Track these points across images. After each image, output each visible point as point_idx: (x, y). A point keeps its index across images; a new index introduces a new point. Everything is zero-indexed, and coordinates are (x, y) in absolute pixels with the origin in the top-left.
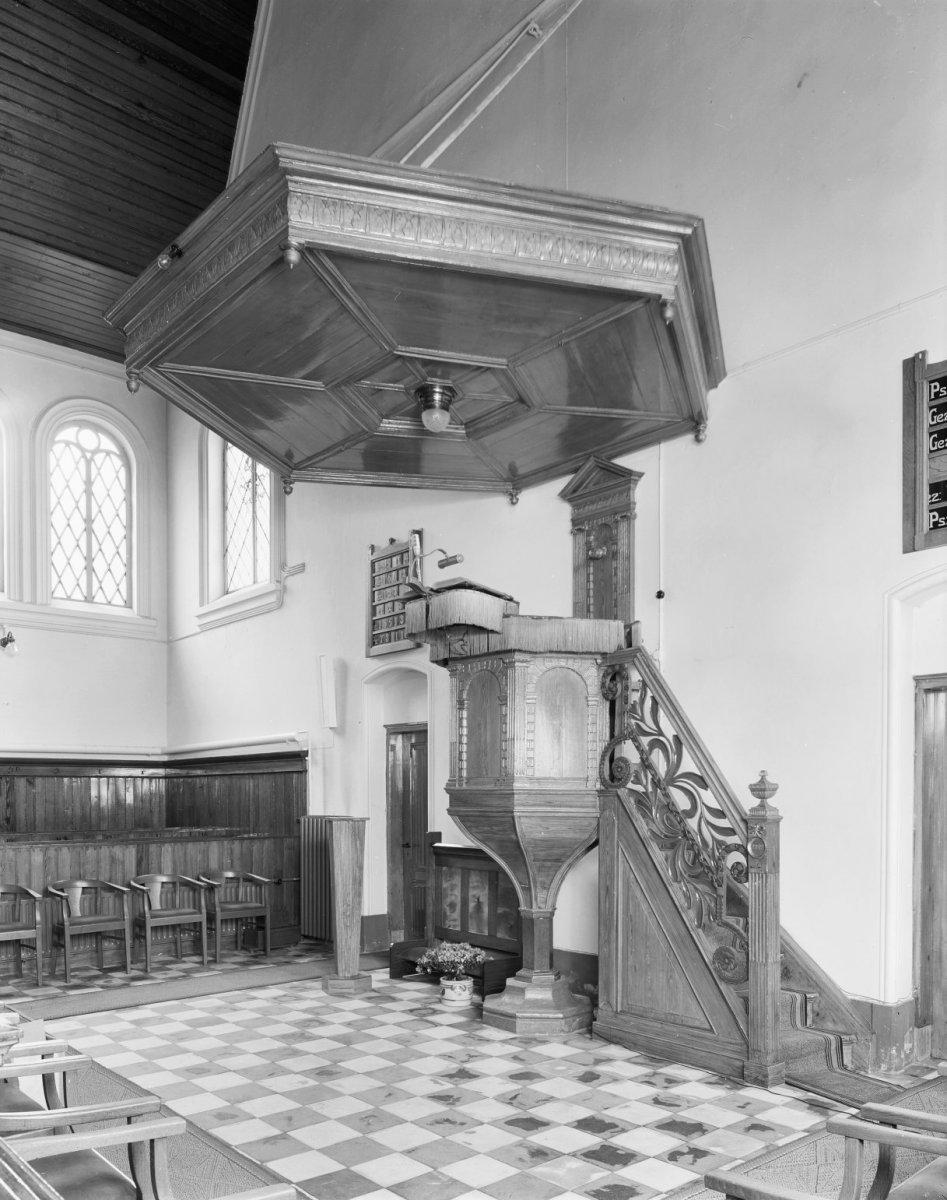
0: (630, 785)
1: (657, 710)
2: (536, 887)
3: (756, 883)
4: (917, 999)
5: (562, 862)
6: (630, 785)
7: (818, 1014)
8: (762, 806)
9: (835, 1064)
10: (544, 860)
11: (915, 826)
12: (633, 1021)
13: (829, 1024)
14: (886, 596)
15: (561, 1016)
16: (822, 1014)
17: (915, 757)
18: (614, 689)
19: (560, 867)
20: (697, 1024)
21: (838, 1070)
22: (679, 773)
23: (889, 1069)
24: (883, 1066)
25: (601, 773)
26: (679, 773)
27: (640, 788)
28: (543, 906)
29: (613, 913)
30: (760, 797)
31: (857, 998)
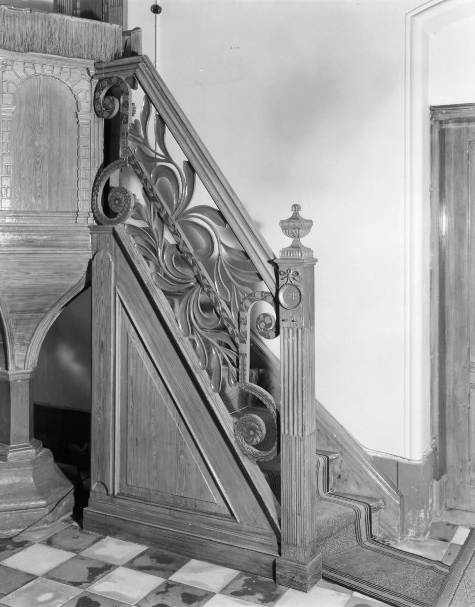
0: (130, 221)
1: (164, 132)
2: (12, 343)
3: (290, 341)
4: (435, 449)
5: (47, 313)
6: (130, 221)
7: (339, 477)
8: (296, 247)
9: (364, 536)
10: (23, 312)
11: (431, 265)
12: (134, 506)
13: (352, 487)
14: (409, 16)
15: (43, 502)
16: (344, 475)
17: (431, 192)
18: (110, 106)
19: (42, 318)
20: (214, 509)
21: (368, 544)
22: (191, 206)
23: (418, 535)
24: (411, 531)
25: (94, 210)
26: (191, 206)
27: (139, 224)
28: (21, 365)
29: (108, 375)
30: (293, 236)
31: (379, 455)
